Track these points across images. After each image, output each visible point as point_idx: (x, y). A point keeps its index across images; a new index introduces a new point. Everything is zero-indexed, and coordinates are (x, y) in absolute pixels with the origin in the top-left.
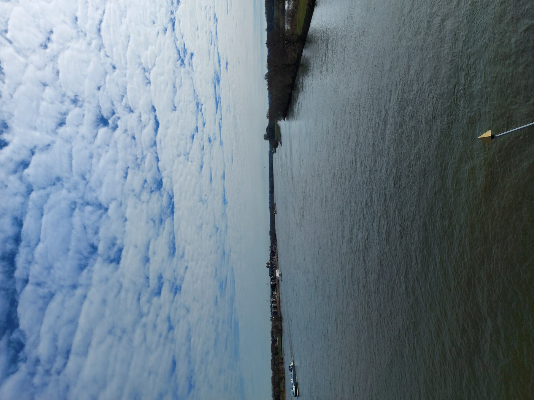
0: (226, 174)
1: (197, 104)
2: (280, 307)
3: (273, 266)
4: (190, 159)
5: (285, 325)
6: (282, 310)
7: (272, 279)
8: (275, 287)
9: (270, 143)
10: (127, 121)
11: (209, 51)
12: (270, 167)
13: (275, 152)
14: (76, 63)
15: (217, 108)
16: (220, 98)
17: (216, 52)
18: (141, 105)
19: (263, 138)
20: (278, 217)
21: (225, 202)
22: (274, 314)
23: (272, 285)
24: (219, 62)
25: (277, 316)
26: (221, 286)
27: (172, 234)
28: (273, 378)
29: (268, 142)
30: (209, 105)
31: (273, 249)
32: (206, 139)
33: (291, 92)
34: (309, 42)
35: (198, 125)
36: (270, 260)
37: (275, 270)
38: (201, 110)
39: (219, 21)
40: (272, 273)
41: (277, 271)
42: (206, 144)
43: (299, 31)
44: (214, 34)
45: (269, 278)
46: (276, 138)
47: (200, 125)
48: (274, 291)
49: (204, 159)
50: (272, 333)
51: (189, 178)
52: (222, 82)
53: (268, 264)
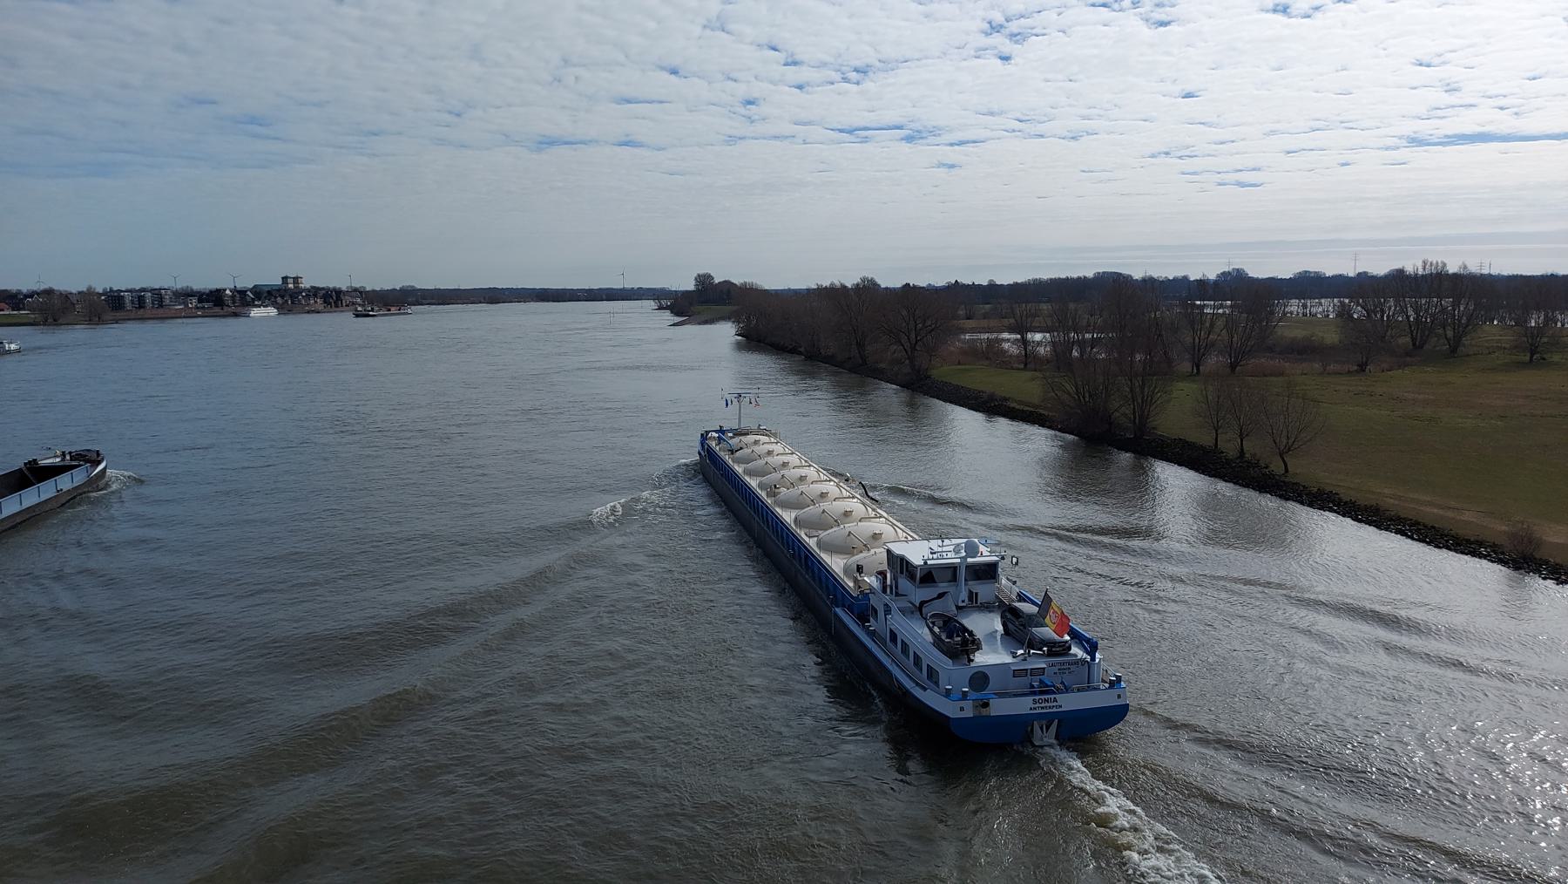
0: (636, 150)
1: (862, 71)
2: (143, 319)
3: (287, 297)
4: (708, 32)
5: (79, 334)
6: (130, 325)
7: (242, 293)
8: (216, 303)
9: (686, 294)
11: (1001, 113)
12: (623, 290)
13: (661, 308)
15: (841, 131)
16: (865, 140)
17: (989, 134)
20: (341, 322)
21: (549, 142)
24: (961, 143)
26: (253, 120)
29: (690, 286)
30: (850, 104)
31: (348, 299)
32: (757, 89)
33: (800, 353)
34: (912, 405)
35: (804, 68)
37: (275, 304)
38: (846, 80)
39: (1072, 143)
40: (263, 295)
41: (272, 311)
42: (741, 90)
43: (942, 372)
44: (1041, 128)
47: (803, 74)
48: (200, 301)
49: (696, 80)
51: (652, 25)
52: (906, 147)
53: (296, 280)
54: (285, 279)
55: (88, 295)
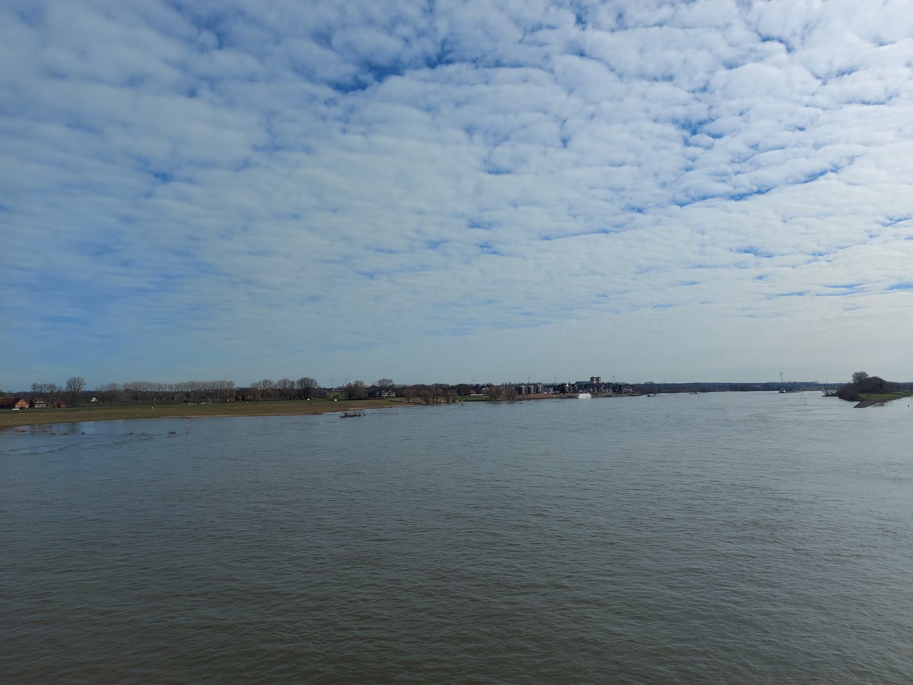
2: (529, 399)
3: (595, 387)
8: (561, 391)
9: (849, 385)
10: (718, 156)
13: (827, 395)
14: (772, 83)
18: (768, 175)
19: (859, 371)
22: (518, 388)
23: (563, 385)
25: (516, 393)
27: (564, 235)
28: (423, 387)
29: (849, 379)
31: (625, 389)
36: (605, 384)
37: (589, 391)
41: (589, 395)
45: (573, 382)
46: (863, 396)
50: (489, 386)
53: (598, 379)
54: (592, 378)
55: (508, 387)
